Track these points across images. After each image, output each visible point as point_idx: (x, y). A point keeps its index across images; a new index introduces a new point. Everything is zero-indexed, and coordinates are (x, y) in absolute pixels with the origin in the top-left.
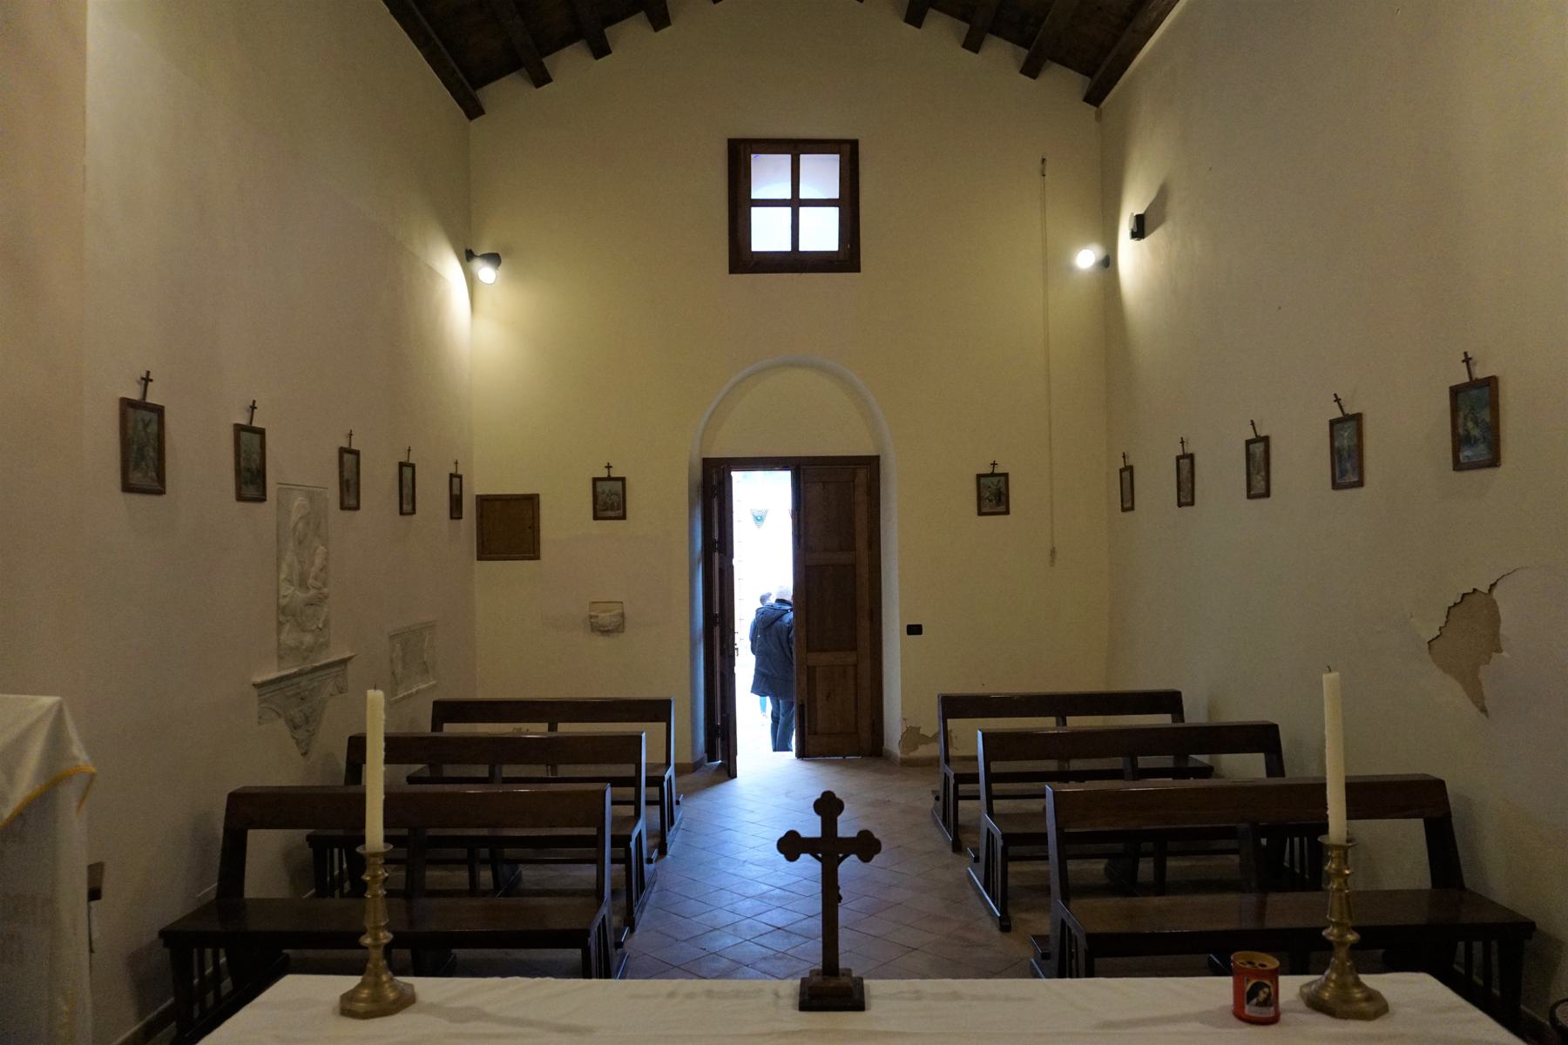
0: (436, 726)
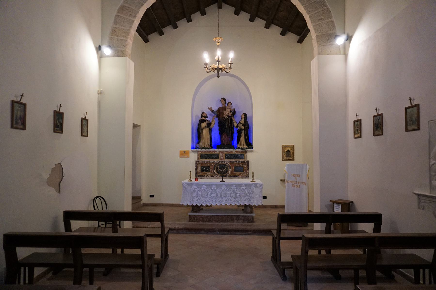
0: (68, 227)
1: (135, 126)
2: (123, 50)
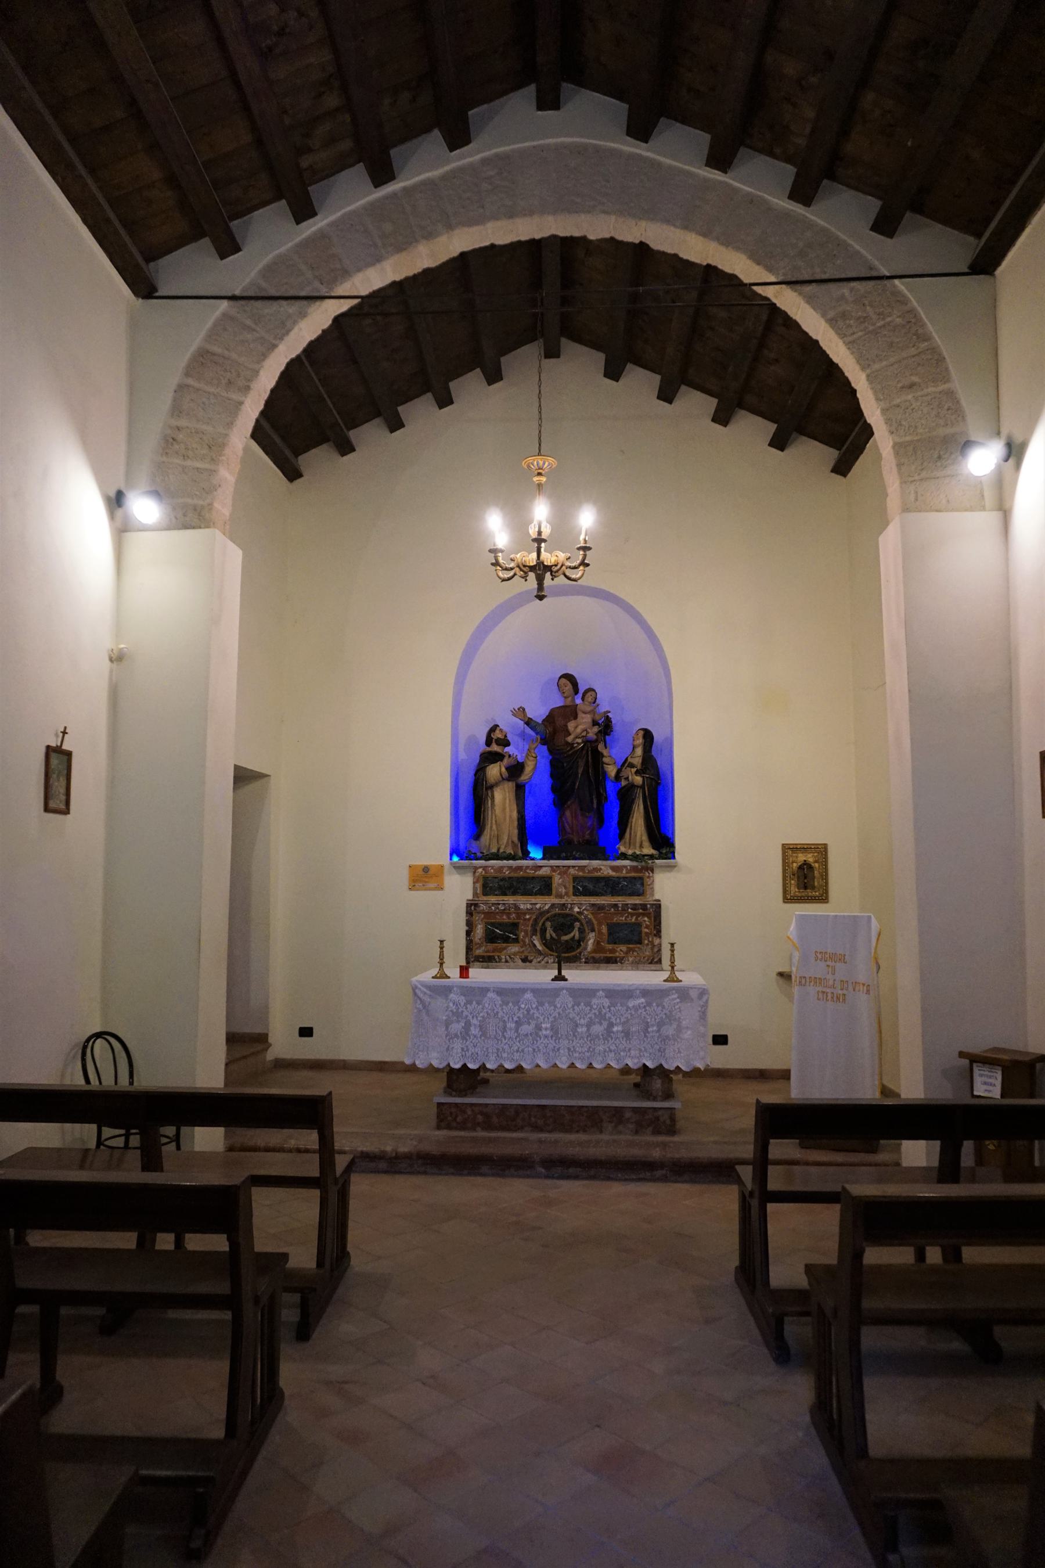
1: (243, 777)
2: (202, 506)
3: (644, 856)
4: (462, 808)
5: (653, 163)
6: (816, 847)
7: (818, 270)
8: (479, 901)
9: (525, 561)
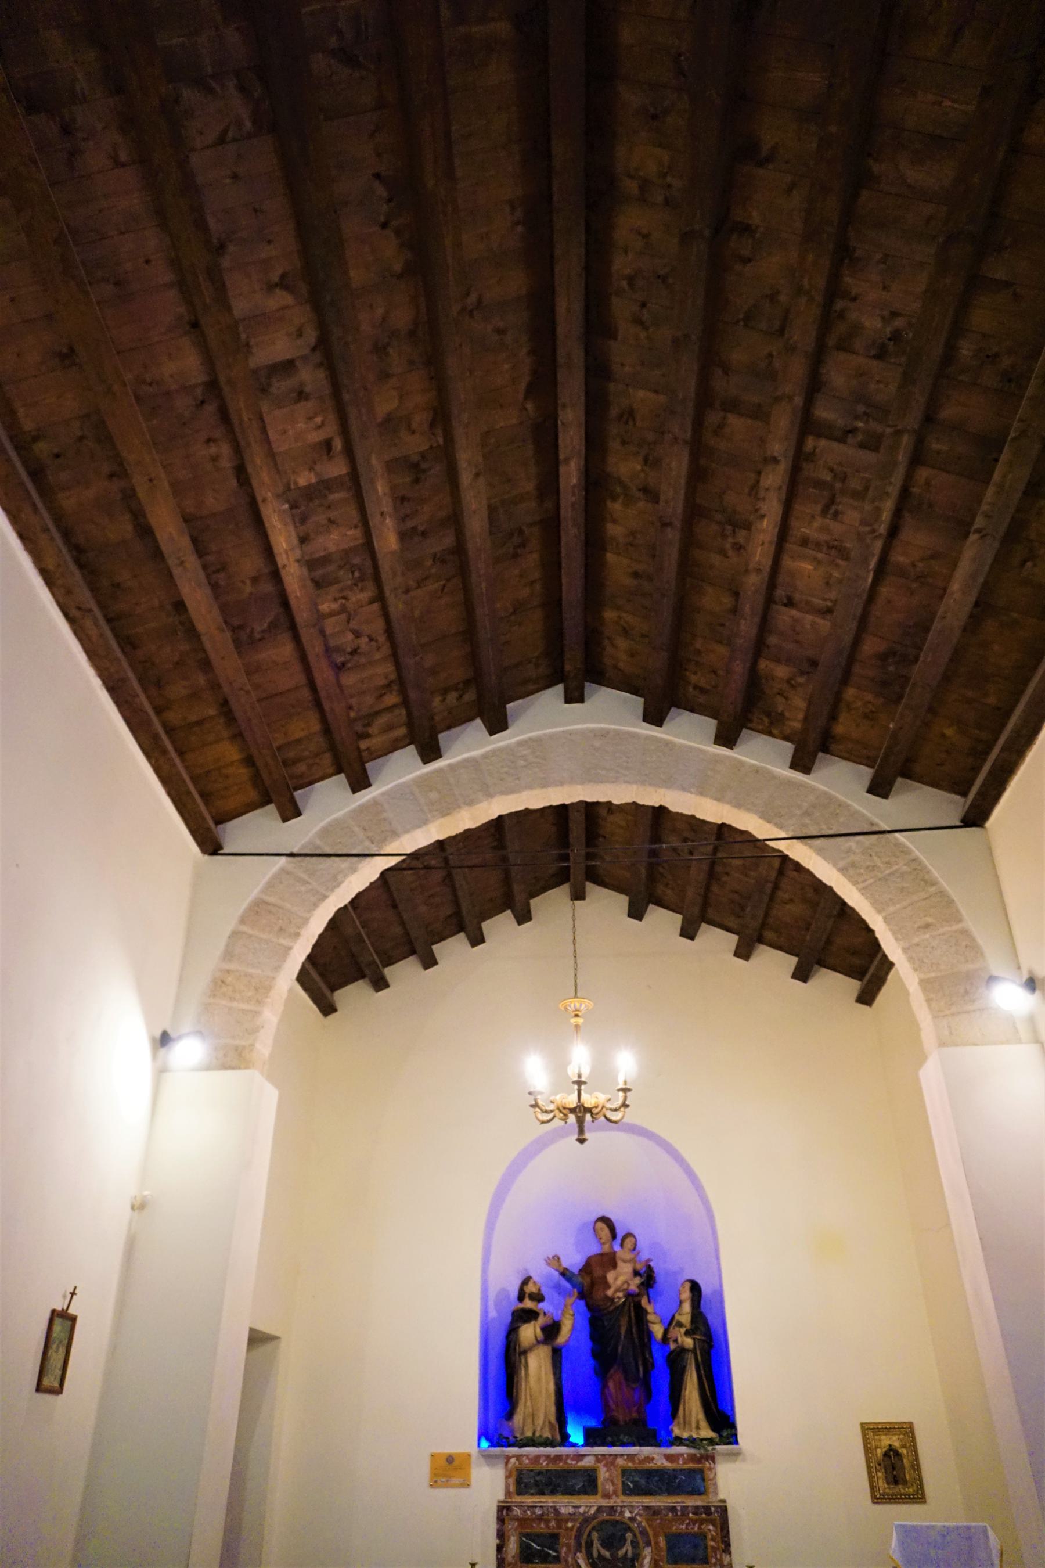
3: (702, 1440)
4: (491, 1382)
5: (667, 743)
6: (900, 1427)
7: (824, 827)
8: (512, 1502)
9: (565, 1104)
